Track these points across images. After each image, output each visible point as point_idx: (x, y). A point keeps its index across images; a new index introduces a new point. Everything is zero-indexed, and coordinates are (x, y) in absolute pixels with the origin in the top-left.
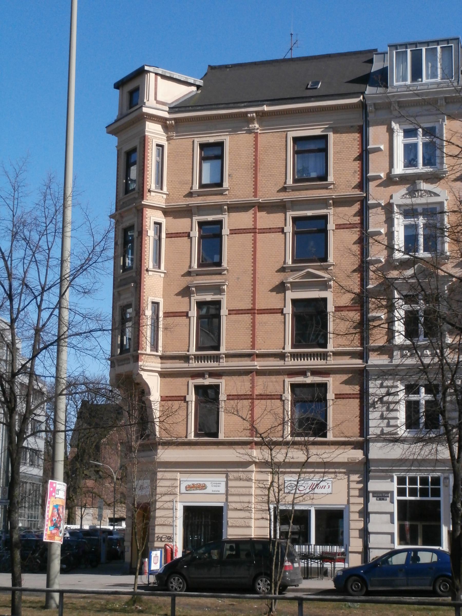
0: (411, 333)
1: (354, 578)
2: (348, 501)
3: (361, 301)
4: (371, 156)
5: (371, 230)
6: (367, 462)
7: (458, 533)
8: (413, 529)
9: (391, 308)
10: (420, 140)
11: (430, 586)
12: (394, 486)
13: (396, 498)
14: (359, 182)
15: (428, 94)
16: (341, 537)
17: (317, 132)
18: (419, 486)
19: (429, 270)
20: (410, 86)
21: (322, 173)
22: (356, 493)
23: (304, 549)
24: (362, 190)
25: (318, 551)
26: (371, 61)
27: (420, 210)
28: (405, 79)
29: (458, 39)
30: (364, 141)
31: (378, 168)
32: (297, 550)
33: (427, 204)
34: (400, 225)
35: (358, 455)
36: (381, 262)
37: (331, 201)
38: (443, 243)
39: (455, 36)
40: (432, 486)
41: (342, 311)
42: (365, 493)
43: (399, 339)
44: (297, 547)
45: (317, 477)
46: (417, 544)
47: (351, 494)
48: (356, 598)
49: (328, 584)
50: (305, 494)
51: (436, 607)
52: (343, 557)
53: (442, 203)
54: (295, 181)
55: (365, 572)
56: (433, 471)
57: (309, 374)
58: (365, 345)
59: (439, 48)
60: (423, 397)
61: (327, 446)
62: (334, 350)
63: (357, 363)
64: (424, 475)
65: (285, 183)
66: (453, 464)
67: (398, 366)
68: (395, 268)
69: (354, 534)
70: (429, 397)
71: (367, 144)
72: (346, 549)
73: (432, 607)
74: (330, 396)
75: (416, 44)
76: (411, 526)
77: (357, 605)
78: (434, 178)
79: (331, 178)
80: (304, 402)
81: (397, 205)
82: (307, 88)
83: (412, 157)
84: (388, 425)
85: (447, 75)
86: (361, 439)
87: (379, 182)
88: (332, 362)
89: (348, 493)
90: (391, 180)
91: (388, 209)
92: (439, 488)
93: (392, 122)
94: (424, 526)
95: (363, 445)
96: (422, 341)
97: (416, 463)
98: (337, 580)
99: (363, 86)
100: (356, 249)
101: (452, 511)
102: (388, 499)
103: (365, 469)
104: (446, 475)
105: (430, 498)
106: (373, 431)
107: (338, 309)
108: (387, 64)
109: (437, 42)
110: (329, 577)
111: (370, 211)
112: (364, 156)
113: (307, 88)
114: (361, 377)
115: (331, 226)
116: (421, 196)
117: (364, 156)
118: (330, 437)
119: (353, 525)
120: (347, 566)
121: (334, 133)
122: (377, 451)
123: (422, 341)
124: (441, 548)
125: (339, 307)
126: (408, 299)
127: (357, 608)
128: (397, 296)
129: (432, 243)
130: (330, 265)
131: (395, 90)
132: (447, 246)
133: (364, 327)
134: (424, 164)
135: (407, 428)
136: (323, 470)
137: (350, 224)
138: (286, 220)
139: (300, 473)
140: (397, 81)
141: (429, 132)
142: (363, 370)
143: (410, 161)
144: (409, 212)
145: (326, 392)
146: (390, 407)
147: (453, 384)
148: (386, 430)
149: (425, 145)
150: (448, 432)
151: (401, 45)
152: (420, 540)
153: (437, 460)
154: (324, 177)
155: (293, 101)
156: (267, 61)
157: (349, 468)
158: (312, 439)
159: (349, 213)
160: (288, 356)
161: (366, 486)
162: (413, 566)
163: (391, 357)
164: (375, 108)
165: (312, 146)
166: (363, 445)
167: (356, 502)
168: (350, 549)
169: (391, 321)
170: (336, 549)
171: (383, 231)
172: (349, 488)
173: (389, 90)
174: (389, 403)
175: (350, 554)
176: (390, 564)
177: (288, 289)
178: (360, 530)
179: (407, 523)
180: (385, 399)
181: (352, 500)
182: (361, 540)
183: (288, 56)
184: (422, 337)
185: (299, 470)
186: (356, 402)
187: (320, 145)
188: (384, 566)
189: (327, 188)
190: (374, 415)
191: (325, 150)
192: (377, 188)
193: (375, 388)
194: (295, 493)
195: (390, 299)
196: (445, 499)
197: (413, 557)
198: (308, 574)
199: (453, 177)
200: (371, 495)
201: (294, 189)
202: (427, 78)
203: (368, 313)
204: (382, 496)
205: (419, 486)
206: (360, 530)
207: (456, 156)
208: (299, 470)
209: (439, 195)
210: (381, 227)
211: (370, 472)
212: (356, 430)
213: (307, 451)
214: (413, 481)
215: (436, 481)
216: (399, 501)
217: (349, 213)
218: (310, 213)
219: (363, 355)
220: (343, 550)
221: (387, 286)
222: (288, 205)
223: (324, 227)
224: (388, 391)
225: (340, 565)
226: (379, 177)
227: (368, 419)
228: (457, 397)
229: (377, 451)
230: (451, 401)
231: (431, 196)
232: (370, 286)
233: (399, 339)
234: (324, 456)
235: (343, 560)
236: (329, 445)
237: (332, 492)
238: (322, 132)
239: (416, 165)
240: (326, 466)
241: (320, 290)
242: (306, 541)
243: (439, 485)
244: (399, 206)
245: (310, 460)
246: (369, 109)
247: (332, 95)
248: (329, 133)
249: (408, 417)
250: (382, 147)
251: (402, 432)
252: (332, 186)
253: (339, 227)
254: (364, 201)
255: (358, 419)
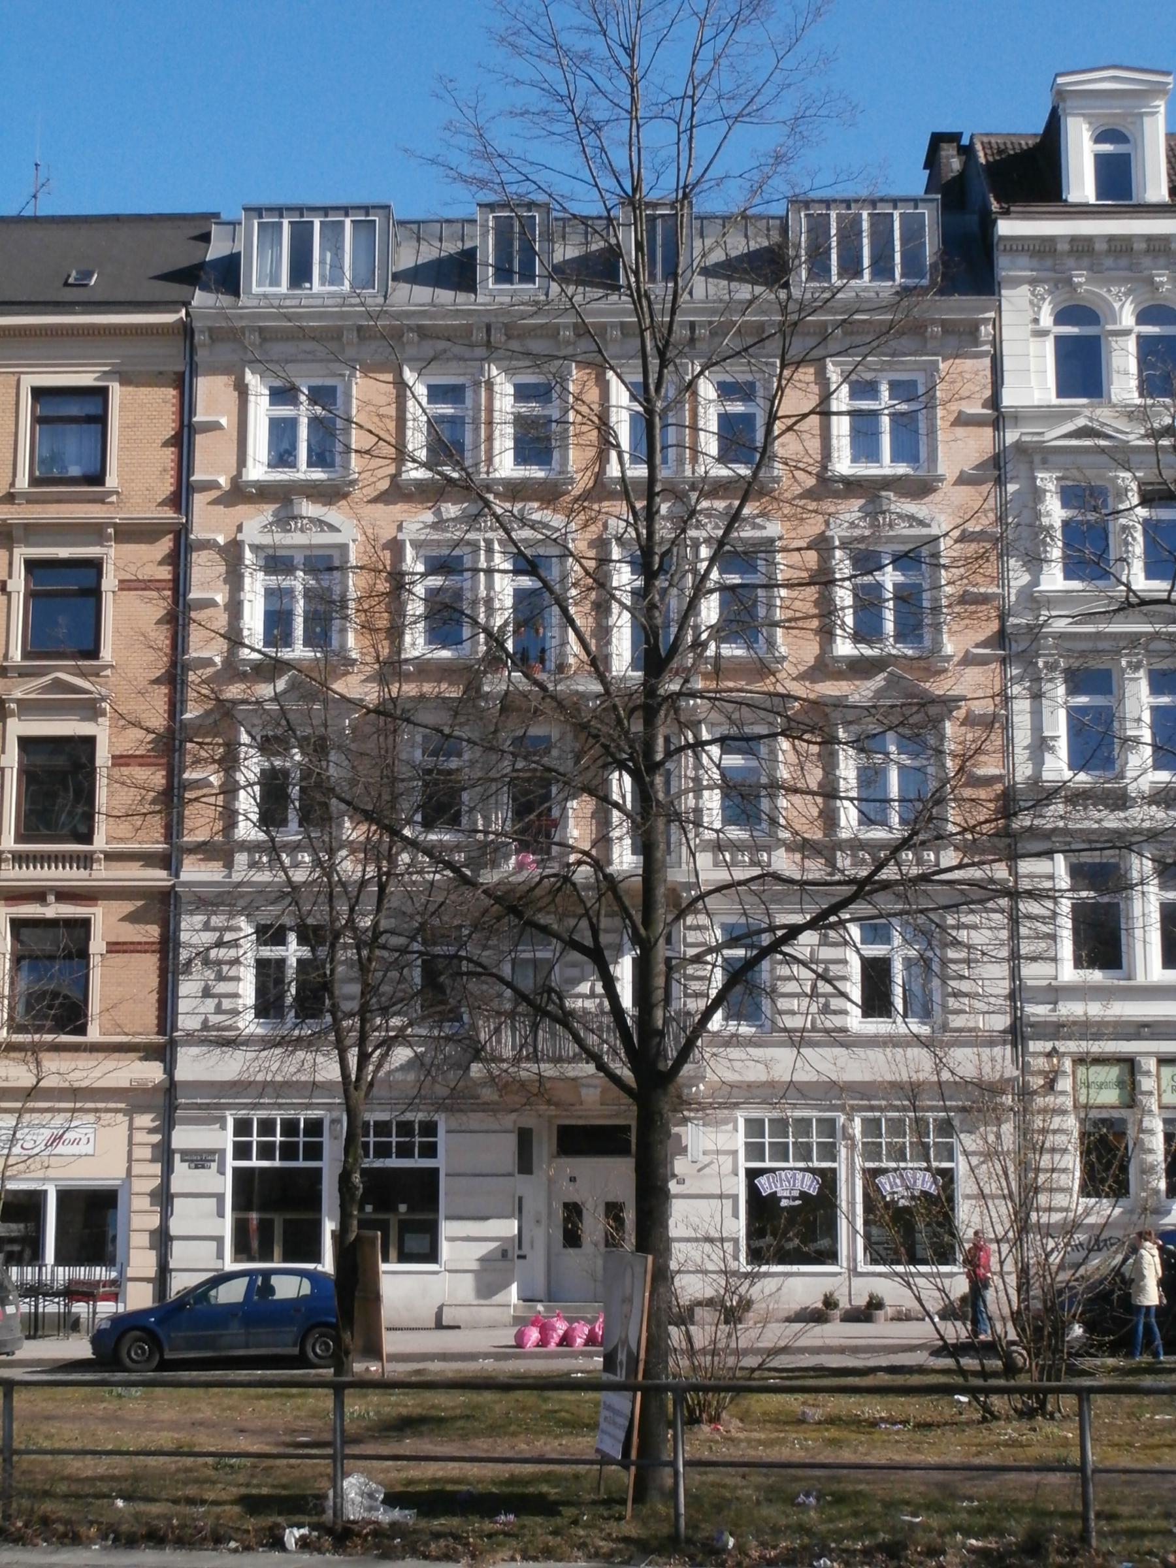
0: (270, 817)
1: (137, 1333)
2: (129, 1170)
3: (170, 746)
4: (199, 439)
5: (194, 595)
6: (171, 1088)
7: (352, 1236)
8: (265, 1227)
9: (229, 762)
10: (303, 413)
11: (295, 1345)
12: (227, 1139)
13: (231, 1163)
14: (173, 493)
15: (321, 316)
16: (110, 1248)
17: (86, 379)
18: (278, 1138)
19: (312, 685)
20: (286, 297)
21: (94, 469)
22: (147, 1153)
23: (30, 1273)
24: (178, 509)
25: (61, 1277)
26: (205, 238)
27: (299, 559)
28: (275, 282)
29: (388, 207)
30: (186, 405)
31: (212, 464)
32: (14, 1278)
33: (310, 547)
34: (255, 587)
35: (153, 1072)
36: (214, 664)
37: (111, 530)
38: (343, 631)
39: (383, 201)
40: (304, 1138)
41: (128, 765)
42: (165, 1154)
43: (247, 830)
44: (14, 1271)
45: (59, 1120)
46: (271, 1260)
47: (135, 1157)
48: (134, 1377)
49: (80, 1348)
50: (30, 1157)
51: (303, 1390)
52: (115, 1291)
53: (344, 548)
54: (34, 481)
55: (157, 1322)
56: (308, 1106)
57: (51, 898)
58: (175, 840)
59: (348, 221)
60: (293, 951)
61: (84, 1055)
62: (107, 848)
63: (157, 877)
64: (290, 1114)
65: (12, 485)
66: (346, 1091)
67: (240, 884)
68: (242, 677)
69: (139, 1240)
70: (305, 952)
71: (192, 412)
72: (121, 1273)
73: (294, 1390)
74: (97, 946)
75: (300, 210)
76: (262, 1222)
77: (136, 1392)
78: (330, 494)
79: (112, 481)
80: (37, 958)
81: (250, 546)
82: (66, 284)
83: (285, 445)
84: (219, 1010)
85: (363, 281)
86: (161, 1039)
87: (214, 494)
88: (103, 874)
89: (130, 1153)
90: (240, 493)
91: (232, 553)
92: (321, 1143)
93: (248, 372)
94: (287, 1222)
95: (164, 1053)
96: (292, 833)
97: (269, 1090)
98: (98, 1340)
99: (186, 288)
100: (161, 637)
101: (340, 1190)
102: (214, 1165)
103: (167, 1103)
104: (335, 1114)
105: (301, 1164)
106: (187, 1022)
107: (119, 760)
108: (240, 247)
109: (346, 210)
110: (83, 1333)
111: (194, 555)
112: (183, 438)
113: (66, 284)
114: (163, 907)
115: (109, 583)
116: (302, 530)
117: (183, 438)
118: (94, 1034)
119: (137, 1221)
120: (121, 1309)
121: (121, 384)
122: (193, 1065)
123: (292, 833)
124: (320, 1267)
125: (122, 757)
126: (266, 746)
127: (136, 1398)
128: (245, 738)
129: (321, 629)
130: (105, 667)
131: (255, 303)
132: (351, 640)
133: (172, 800)
134: (310, 464)
135: (257, 1016)
136: (71, 1105)
137: (138, 580)
138: (11, 564)
139: (20, 1112)
140: (259, 285)
141: (320, 395)
142: (169, 893)
143: (282, 457)
144: (276, 563)
145: (88, 938)
146: (221, 970)
147: (351, 923)
148: (214, 1019)
149: (314, 421)
150: (336, 1027)
151: (270, 209)
152: (277, 1251)
153: (314, 1083)
154: (98, 478)
155: (36, 308)
156: (77, 217)
157: (133, 1099)
158: (49, 1038)
159: (149, 559)
160: (7, 860)
161: (167, 1139)
162: (260, 1305)
163: (229, 865)
164: (211, 337)
165: (73, 409)
166: (164, 1053)
167: (145, 1173)
168: (130, 1273)
169: (230, 790)
170: (99, 1273)
171: (220, 598)
172: (130, 1143)
173: (244, 300)
174: (219, 962)
175: (130, 1285)
176: (213, 1301)
177: (12, 715)
178: (152, 1233)
179: (254, 1216)
180: (213, 953)
181: (137, 1169)
182: (154, 1253)
183: (28, 212)
184: (293, 825)
185: (19, 1105)
186: (151, 962)
187: (90, 408)
188: (199, 1307)
189: (103, 502)
190: (188, 988)
191: (101, 420)
192: (210, 507)
193: (193, 932)
194: (8, 1156)
195: (232, 747)
196: (330, 1166)
197: (261, 1287)
198: (36, 1330)
199: (372, 492)
200: (177, 1157)
201: (31, 499)
202: (323, 284)
203: (182, 770)
204: (200, 1159)
205: (278, 1138)
206: (152, 1233)
207: (367, 452)
208: (19, 1105)
209: (336, 530)
210: (216, 591)
211: (176, 1108)
212: (151, 1019)
213: (38, 1064)
214: (267, 1127)
215: (315, 1127)
216: (236, 1170)
217: (149, 559)
218: (63, 553)
219: (168, 861)
220: (114, 1275)
221: (224, 715)
222: (16, 533)
223: (93, 585)
224: (221, 937)
225: (106, 1308)
226: (214, 485)
227: (176, 997)
228: (359, 953)
229: (193, 1065)
230: (348, 963)
231: (322, 531)
232: (187, 716)
233: (247, 830)
234: (77, 1075)
235: (115, 1297)
236: (85, 1050)
237: (92, 1151)
238: (96, 379)
239: (293, 465)
240: (79, 1097)
241: (82, 720)
242: (36, 1257)
243: (321, 1136)
244: (255, 548)
245: (42, 1084)
246: (199, 338)
247: (46, 303)
248: (110, 384)
249: (261, 991)
250: (224, 421)
251: (248, 1024)
252: (114, 498)
253: (126, 585)
254: (181, 534)
255: (155, 996)
